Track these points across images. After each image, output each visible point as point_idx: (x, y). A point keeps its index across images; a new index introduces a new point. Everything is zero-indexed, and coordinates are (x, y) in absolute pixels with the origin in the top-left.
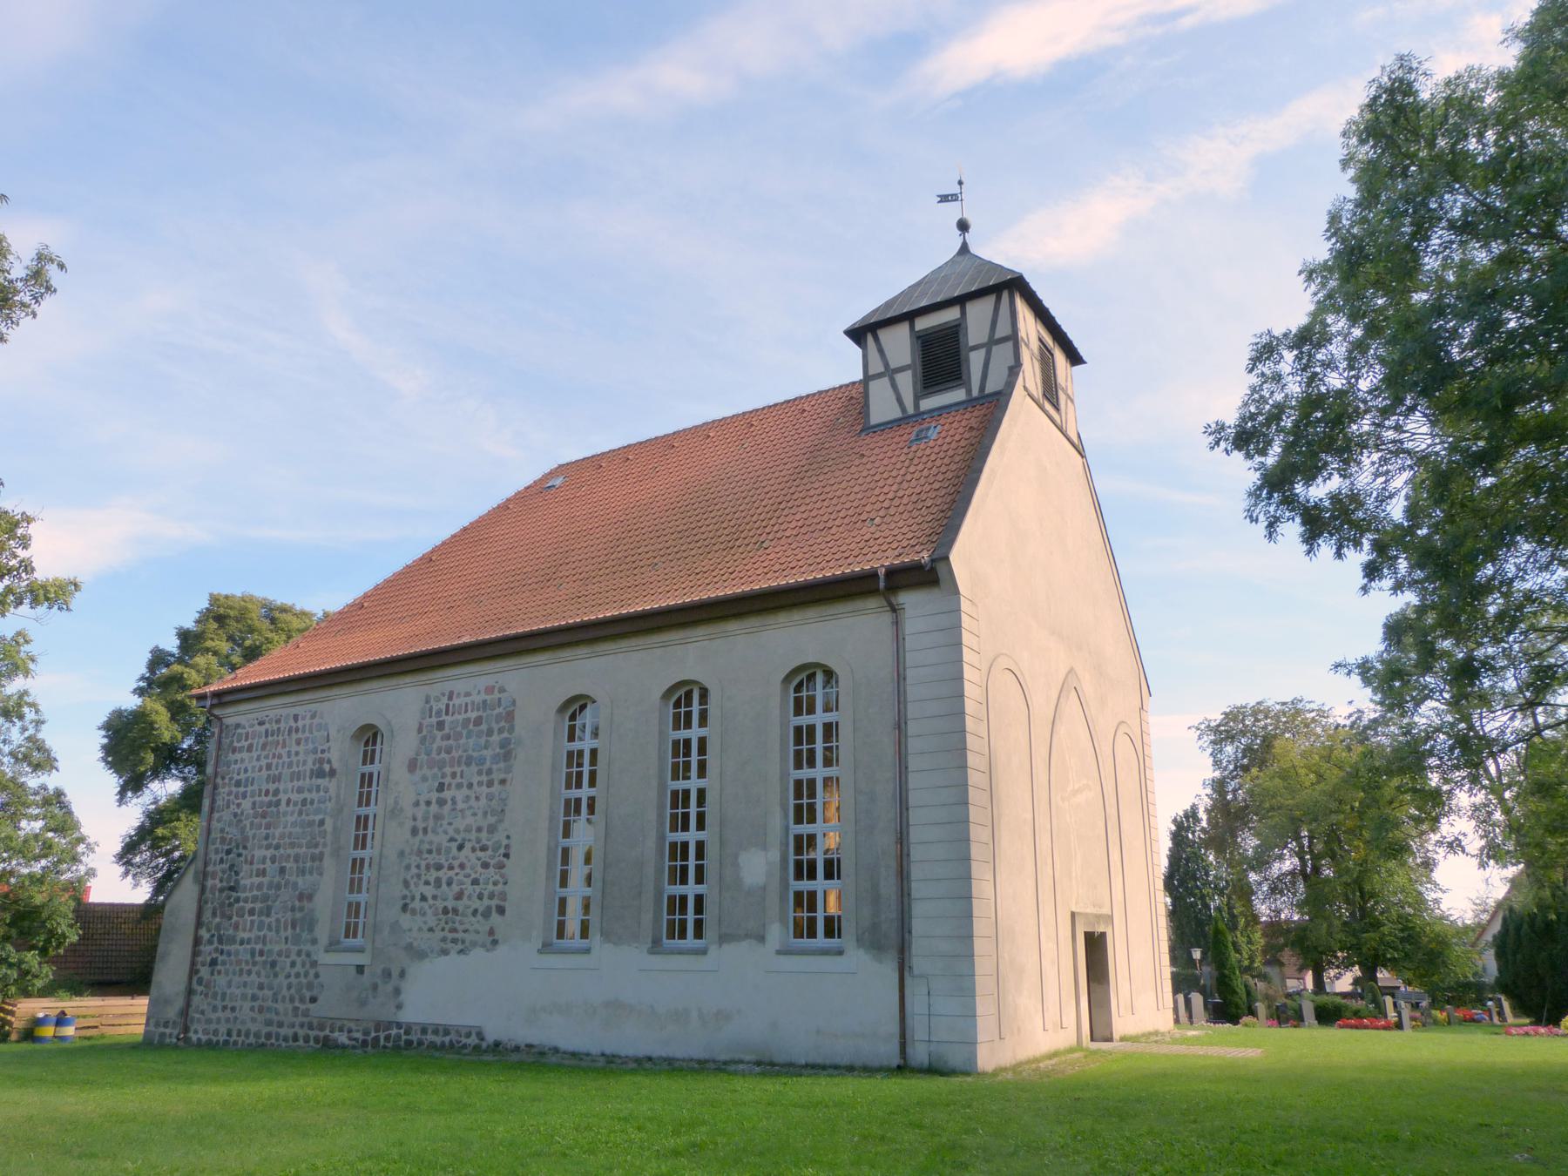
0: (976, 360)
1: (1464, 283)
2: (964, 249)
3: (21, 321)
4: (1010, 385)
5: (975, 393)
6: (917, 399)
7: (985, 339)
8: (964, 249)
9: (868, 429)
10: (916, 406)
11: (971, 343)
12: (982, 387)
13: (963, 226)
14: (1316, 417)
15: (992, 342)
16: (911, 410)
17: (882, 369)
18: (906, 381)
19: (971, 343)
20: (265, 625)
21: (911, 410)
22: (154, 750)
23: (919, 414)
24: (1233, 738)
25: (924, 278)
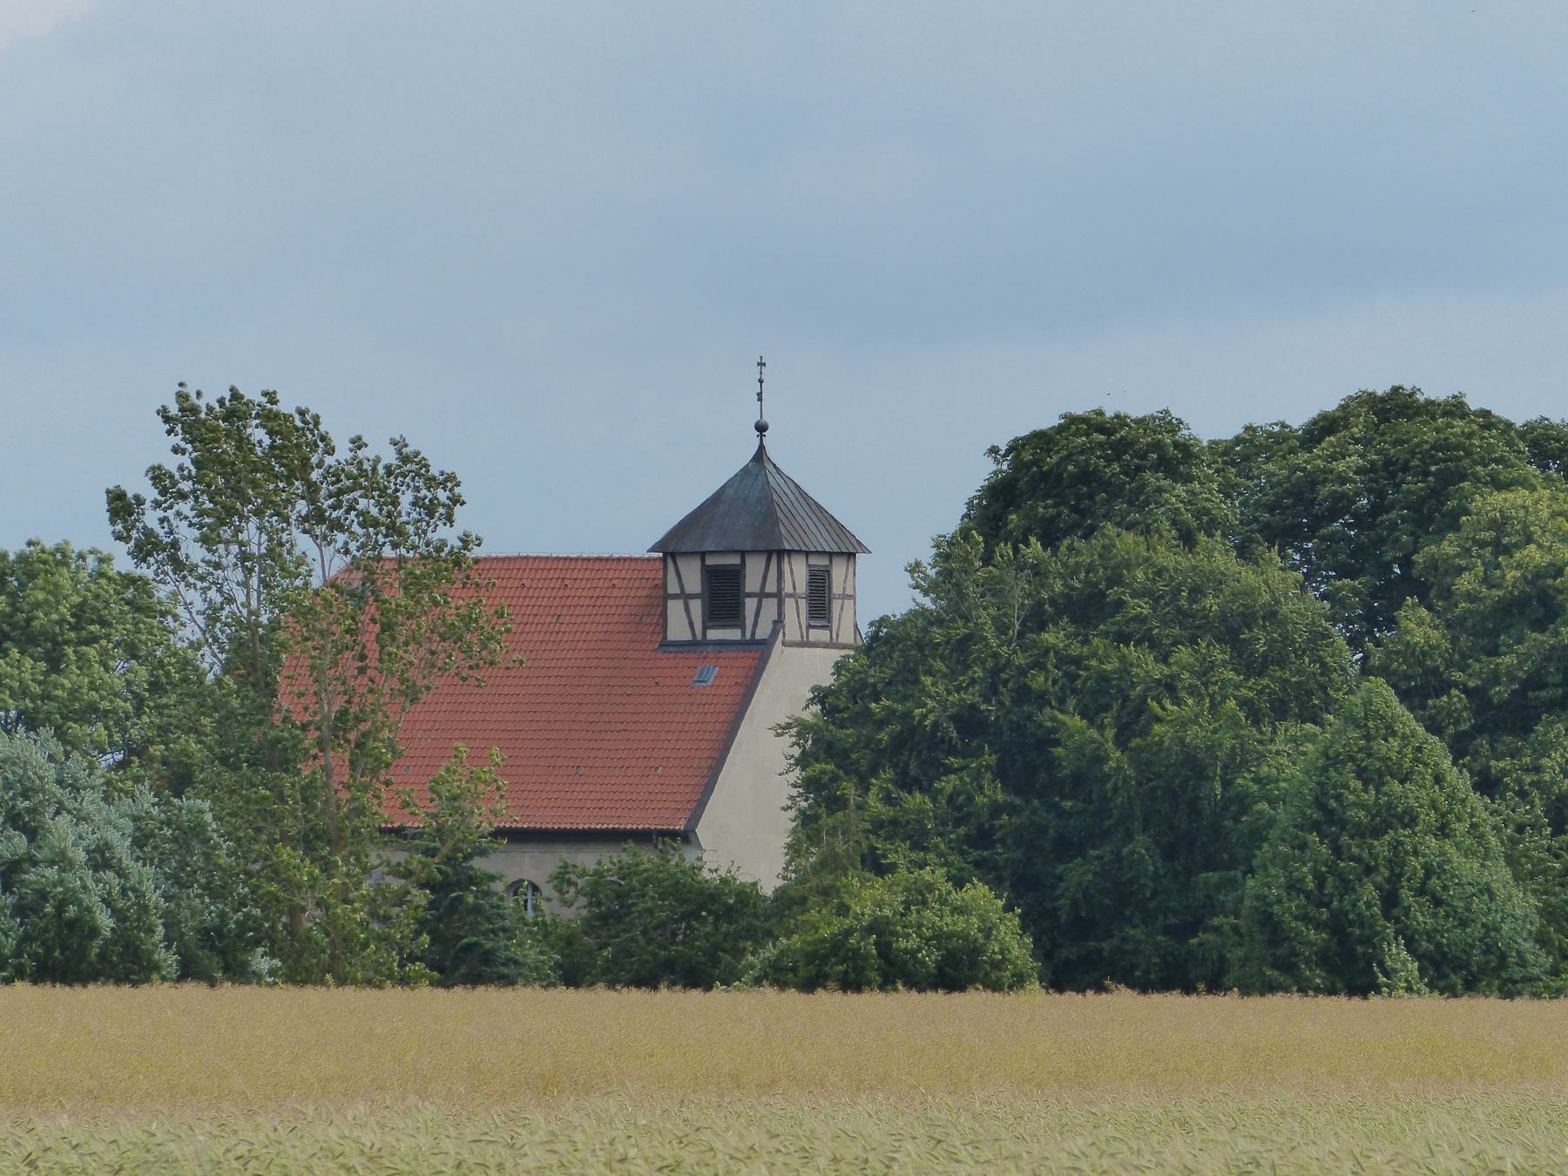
0: (750, 605)
1: (244, 416)
2: (760, 455)
3: (990, 460)
4: (774, 633)
5: (748, 636)
6: (705, 629)
7: (757, 590)
8: (760, 455)
9: (665, 645)
10: (704, 634)
11: (747, 591)
12: (753, 633)
13: (761, 428)
14: (606, 959)
15: (762, 595)
16: (699, 637)
17: (678, 592)
18: (696, 606)
19: (747, 591)
20: (32, 548)
21: (699, 637)
22: (1088, 728)
23: (706, 643)
24: (334, 729)
25: (723, 488)
